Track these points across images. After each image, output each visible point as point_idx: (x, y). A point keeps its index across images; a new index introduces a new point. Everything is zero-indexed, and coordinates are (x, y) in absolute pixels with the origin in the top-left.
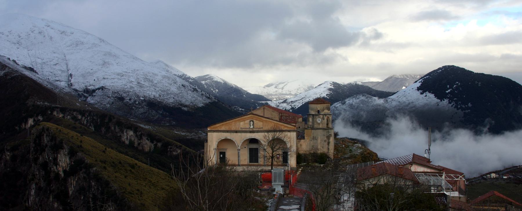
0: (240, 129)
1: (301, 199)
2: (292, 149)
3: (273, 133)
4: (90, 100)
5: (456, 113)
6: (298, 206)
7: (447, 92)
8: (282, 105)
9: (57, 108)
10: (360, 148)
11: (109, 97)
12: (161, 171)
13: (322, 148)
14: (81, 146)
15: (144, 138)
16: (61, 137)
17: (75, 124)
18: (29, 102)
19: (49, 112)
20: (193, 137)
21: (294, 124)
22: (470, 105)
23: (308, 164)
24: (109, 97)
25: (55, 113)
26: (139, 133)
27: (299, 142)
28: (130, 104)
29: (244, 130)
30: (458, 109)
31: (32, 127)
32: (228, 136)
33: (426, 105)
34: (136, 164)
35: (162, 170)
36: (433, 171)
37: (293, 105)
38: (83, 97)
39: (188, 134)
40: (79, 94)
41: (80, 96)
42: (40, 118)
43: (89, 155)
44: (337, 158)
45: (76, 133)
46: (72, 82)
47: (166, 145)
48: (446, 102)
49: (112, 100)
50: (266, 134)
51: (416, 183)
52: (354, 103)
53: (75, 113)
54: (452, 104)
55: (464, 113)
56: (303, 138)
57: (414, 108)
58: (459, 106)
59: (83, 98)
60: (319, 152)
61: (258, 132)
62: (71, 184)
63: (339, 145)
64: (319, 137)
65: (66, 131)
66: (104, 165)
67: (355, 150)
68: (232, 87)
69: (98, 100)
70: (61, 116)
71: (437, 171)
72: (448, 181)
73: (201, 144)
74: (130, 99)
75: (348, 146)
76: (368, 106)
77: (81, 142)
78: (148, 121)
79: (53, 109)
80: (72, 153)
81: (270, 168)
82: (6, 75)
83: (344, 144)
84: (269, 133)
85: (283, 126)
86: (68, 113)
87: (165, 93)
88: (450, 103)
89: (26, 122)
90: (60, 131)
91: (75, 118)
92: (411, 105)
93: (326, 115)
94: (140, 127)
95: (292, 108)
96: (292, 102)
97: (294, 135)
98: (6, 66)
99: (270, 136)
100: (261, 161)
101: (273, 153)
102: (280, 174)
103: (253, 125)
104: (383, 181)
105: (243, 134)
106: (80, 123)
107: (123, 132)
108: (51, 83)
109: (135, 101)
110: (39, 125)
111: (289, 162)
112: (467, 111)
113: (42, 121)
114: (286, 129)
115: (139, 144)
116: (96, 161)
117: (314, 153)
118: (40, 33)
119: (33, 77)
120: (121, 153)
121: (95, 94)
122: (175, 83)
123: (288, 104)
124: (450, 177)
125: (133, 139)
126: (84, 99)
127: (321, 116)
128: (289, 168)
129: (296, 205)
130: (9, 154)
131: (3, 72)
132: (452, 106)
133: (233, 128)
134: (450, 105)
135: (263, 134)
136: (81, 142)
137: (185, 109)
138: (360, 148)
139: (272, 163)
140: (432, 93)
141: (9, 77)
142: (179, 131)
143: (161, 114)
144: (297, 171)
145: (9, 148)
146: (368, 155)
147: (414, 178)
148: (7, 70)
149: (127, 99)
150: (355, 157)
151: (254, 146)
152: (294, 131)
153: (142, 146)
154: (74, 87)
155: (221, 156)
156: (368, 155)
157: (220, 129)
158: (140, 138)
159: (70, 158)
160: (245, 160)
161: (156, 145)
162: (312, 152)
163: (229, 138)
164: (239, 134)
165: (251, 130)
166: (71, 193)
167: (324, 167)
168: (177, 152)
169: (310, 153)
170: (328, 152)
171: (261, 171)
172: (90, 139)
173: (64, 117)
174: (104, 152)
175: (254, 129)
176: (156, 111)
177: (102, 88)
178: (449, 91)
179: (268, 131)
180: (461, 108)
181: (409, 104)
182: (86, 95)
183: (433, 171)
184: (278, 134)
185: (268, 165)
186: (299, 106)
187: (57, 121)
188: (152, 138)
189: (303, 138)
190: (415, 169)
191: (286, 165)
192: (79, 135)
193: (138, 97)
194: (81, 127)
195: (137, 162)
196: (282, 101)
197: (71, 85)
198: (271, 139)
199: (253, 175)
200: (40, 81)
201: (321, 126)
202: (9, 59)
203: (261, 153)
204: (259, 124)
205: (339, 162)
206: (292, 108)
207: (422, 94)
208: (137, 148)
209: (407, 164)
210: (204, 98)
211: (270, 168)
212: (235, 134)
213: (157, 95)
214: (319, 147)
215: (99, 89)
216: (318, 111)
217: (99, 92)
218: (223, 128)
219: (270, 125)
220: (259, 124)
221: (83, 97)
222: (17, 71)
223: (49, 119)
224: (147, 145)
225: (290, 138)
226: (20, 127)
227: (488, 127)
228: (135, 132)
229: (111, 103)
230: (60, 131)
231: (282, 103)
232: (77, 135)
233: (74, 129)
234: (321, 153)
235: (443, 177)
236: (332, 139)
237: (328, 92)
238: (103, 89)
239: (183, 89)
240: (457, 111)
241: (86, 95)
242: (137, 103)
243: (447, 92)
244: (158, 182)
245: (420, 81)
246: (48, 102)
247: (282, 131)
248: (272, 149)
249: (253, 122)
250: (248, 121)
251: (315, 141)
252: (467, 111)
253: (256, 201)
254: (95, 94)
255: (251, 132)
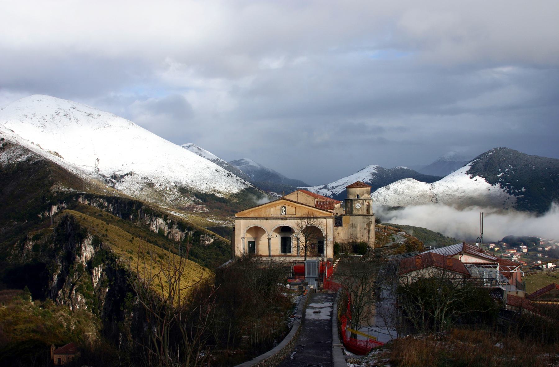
0: (270, 216)
1: (334, 295)
2: (328, 238)
3: (306, 221)
4: (119, 187)
5: (509, 198)
6: (331, 304)
7: (499, 176)
8: (322, 190)
9: (83, 194)
10: (404, 236)
11: (138, 183)
12: (193, 262)
13: (361, 238)
14: (106, 235)
15: (175, 226)
16: (85, 226)
17: (101, 211)
18: (54, 189)
19: (74, 199)
20: (227, 225)
21: (331, 211)
22: (523, 189)
23: (346, 254)
24: (138, 183)
25: (80, 200)
26: (171, 222)
27: (336, 230)
28: (161, 191)
29: (275, 216)
30: (510, 195)
31: (56, 214)
32: (258, 223)
33: (476, 190)
34: (165, 255)
35: (193, 260)
36: (485, 262)
37: (334, 190)
38: (110, 183)
39: (222, 222)
40: (106, 180)
41: (107, 182)
42: (64, 205)
43: (115, 244)
44: (379, 249)
45: (101, 221)
46: (99, 167)
47: (198, 234)
48: (498, 186)
49: (141, 186)
50: (299, 221)
51: (467, 275)
52: (399, 189)
53: (101, 200)
54: (505, 188)
55: (518, 198)
56: (341, 225)
57: (463, 194)
58: (512, 191)
59: (111, 184)
60: (358, 241)
61: (290, 218)
62: (96, 275)
63: (381, 233)
64: (358, 225)
65: (90, 219)
66: (130, 255)
67: (398, 239)
68: (269, 172)
69: (127, 186)
70: (87, 202)
71: (490, 262)
72: (503, 273)
73: (230, 233)
74: (160, 185)
75: (391, 235)
76: (413, 191)
77: (107, 230)
78: (181, 209)
79: (78, 196)
80: (96, 243)
81: (303, 259)
82: (29, 160)
83: (387, 232)
84: (303, 220)
85: (318, 212)
86: (94, 200)
87: (198, 178)
88: (502, 187)
89: (50, 210)
90: (84, 219)
91: (101, 206)
92: (460, 190)
93: (365, 200)
94: (171, 215)
95: (333, 194)
96: (333, 187)
97: (330, 222)
98: (29, 151)
99: (304, 224)
100: (294, 251)
101: (306, 242)
102: (314, 266)
103: (285, 211)
104: (428, 273)
105: (274, 221)
106: (107, 211)
107: (152, 220)
108: (77, 169)
109: (166, 187)
110: (62, 212)
111: (325, 252)
112: (520, 196)
113: (66, 209)
114: (321, 215)
115: (169, 233)
116: (122, 251)
117: (353, 242)
118: (65, 115)
119: (59, 163)
120: (150, 242)
121: (123, 180)
122: (208, 168)
123: (329, 189)
124: (505, 269)
125: (163, 227)
126: (112, 185)
127: (361, 201)
128: (325, 260)
129: (328, 302)
130: (31, 243)
131: (26, 157)
132: (504, 191)
133: (263, 215)
134: (503, 190)
135: (296, 221)
136: (107, 230)
137: (219, 195)
138: (404, 236)
139: (306, 253)
140: (483, 177)
141: (32, 162)
142: (212, 219)
143: (194, 201)
144: (334, 262)
145: (31, 237)
146: (413, 244)
147: (464, 270)
148: (30, 154)
149: (157, 186)
150: (399, 246)
151: (287, 235)
152: (330, 217)
153: (173, 236)
154: (100, 173)
155: (251, 245)
156: (413, 244)
157: (248, 216)
158: (170, 226)
159: (95, 248)
160: (276, 250)
161: (187, 234)
162: (351, 241)
163: (258, 225)
164: (270, 221)
165: (283, 217)
166: (95, 285)
167: (364, 258)
168: (210, 241)
169: (349, 243)
170: (368, 241)
171: (294, 262)
172: (117, 227)
173: (89, 204)
174: (131, 241)
175: (287, 216)
176: (188, 198)
177: (131, 174)
178: (501, 175)
179: (302, 218)
180: (514, 193)
181: (458, 189)
182: (113, 180)
183: (485, 262)
184: (311, 222)
185: (301, 256)
186: (340, 192)
187: (82, 209)
188: (182, 226)
189: (341, 225)
190: (466, 260)
191: (320, 256)
192: (105, 223)
193: (169, 182)
194: (108, 215)
195: (166, 252)
196: (322, 187)
197: (98, 170)
198: (304, 227)
199: (283, 269)
200: (64, 166)
201: (360, 213)
202: (33, 143)
203: (294, 242)
204: (291, 210)
205: (381, 251)
206: (333, 194)
207: (471, 178)
208: (167, 237)
209: (456, 254)
210: (239, 183)
211: (303, 259)
212: (265, 221)
213: (189, 181)
214: (358, 235)
215: (127, 174)
216: (358, 195)
217: (128, 178)
218: (252, 215)
219: (303, 211)
220: (291, 210)
221: (110, 183)
222: (40, 156)
223: (75, 206)
224: (178, 235)
225: (326, 225)
226: (43, 215)
227: (31, 298)
228: (165, 219)
229: (140, 189)
230: (84, 219)
231: (323, 188)
232: (102, 223)
233: (100, 216)
234: (360, 242)
235: (498, 269)
236: (373, 227)
237: (371, 177)
238: (131, 175)
239: (216, 173)
240: (510, 196)
241: (113, 180)
242: (168, 189)
243: (499, 176)
244: (188, 273)
245: (470, 164)
246: (74, 189)
247: (316, 218)
248: (306, 238)
249: (285, 208)
250: (279, 207)
251: (354, 229)
252: (520, 196)
253: (283, 297)
254: (123, 180)
255: (282, 219)
